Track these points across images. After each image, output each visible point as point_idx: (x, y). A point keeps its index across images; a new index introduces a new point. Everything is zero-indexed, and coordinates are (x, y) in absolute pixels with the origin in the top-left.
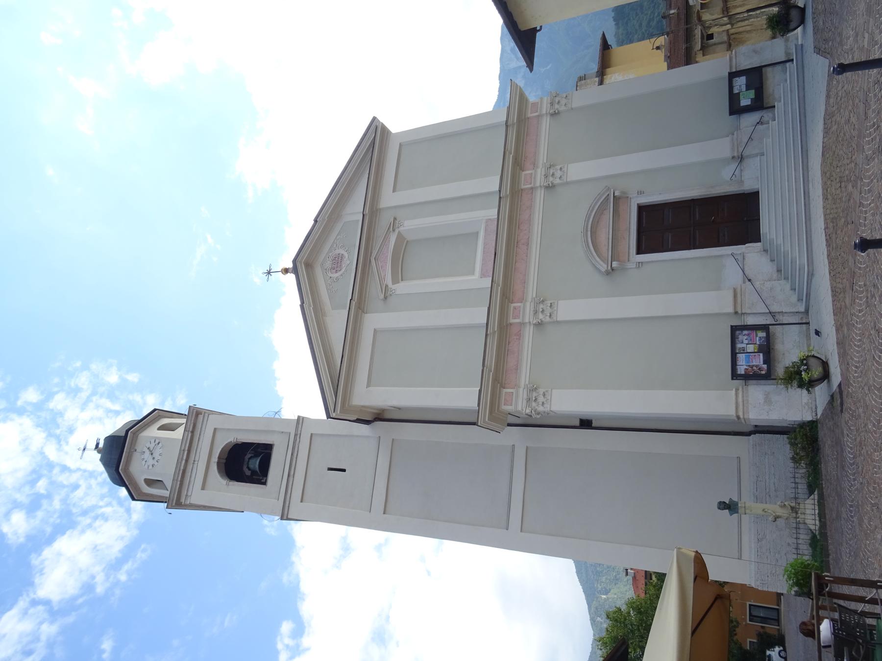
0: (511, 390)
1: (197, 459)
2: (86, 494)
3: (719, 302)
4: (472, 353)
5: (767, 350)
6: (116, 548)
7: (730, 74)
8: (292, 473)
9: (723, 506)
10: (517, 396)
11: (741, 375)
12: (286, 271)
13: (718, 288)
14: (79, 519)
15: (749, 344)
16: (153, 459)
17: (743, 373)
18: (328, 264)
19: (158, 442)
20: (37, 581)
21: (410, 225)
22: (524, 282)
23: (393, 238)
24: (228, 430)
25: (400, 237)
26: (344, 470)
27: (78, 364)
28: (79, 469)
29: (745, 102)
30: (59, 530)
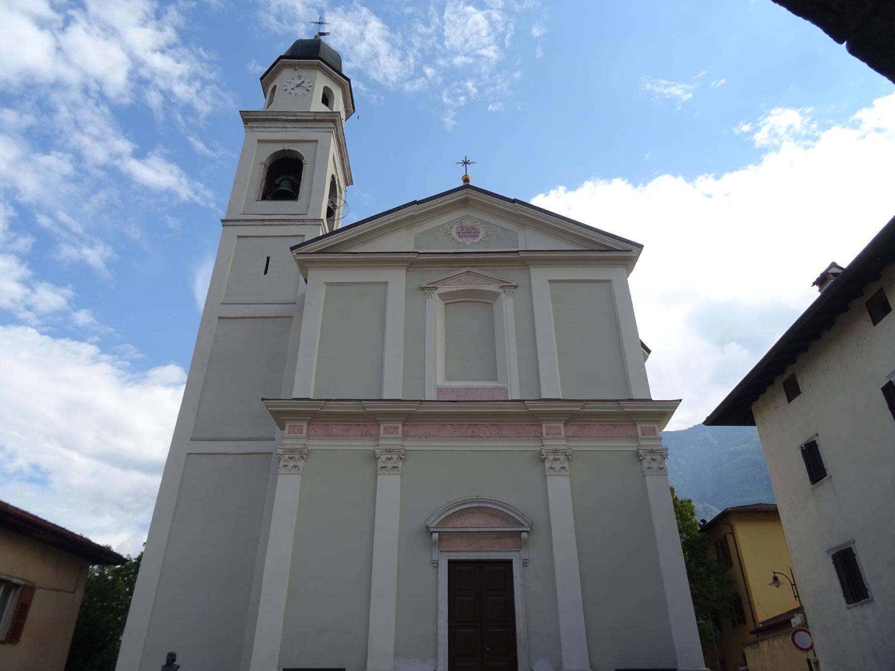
0: (305, 431)
1: (288, 130)
2: (420, 35)
4: (353, 387)
6: (377, 76)
10: (559, 439)
12: (466, 180)
13: (396, 655)
14: (399, 33)
16: (309, 90)
18: (468, 223)
19: (309, 90)
20: (339, 9)
21: (507, 305)
22: (427, 436)
25: (495, 295)
26: (266, 273)
30: (385, 18)
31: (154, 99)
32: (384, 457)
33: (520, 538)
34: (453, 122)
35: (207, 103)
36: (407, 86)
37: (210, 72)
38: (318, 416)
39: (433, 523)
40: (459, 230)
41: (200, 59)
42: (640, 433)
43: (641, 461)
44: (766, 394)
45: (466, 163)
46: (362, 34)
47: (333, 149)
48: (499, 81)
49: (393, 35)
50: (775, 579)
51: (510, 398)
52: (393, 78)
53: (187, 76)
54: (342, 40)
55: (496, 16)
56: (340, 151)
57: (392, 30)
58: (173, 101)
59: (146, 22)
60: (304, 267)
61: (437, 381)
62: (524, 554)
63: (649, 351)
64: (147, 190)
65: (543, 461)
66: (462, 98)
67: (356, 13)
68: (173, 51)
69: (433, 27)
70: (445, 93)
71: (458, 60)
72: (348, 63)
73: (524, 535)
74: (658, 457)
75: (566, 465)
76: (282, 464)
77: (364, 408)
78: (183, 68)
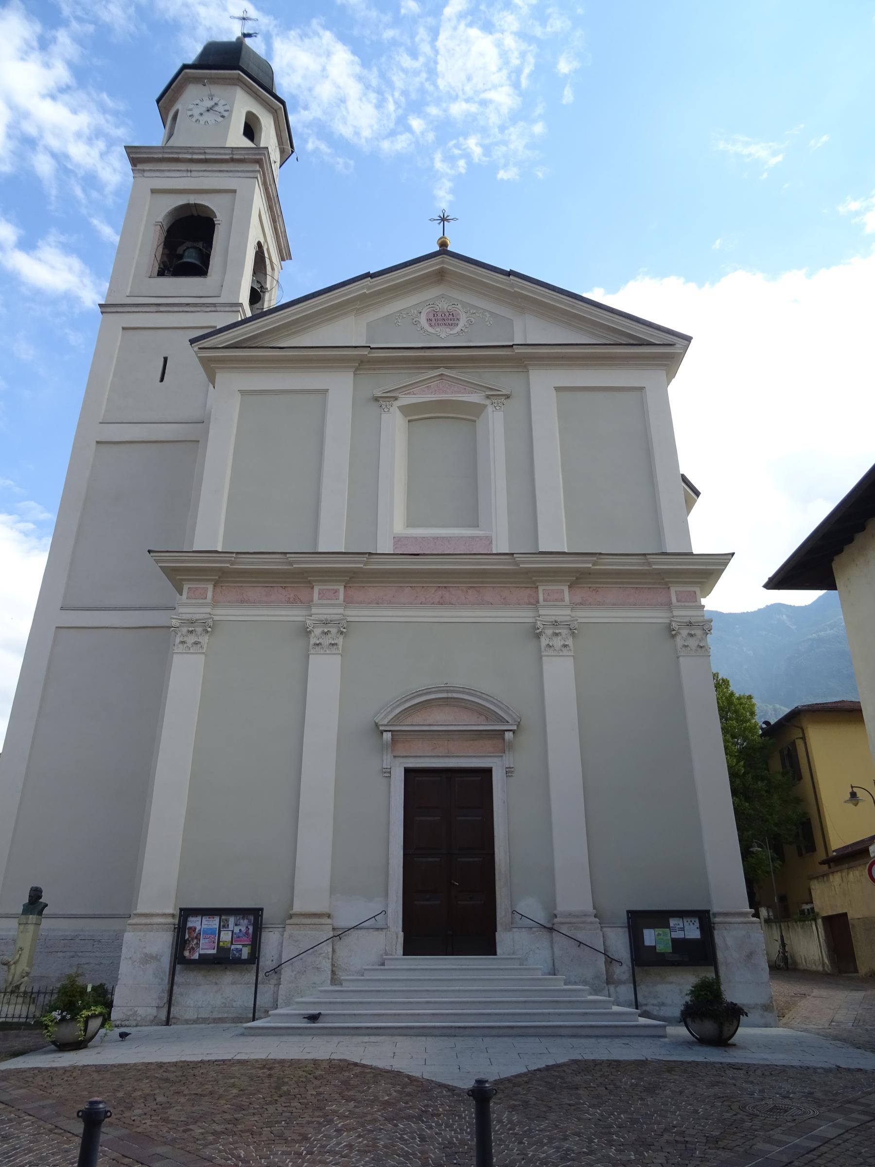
0: (210, 595)
1: (193, 174)
2: (405, 71)
3: (312, 888)
4: (279, 536)
5: (222, 961)
6: (345, 130)
8: (162, 309)
9: (36, 895)
11: (185, 922)
13: (333, 890)
14: (375, 69)
15: (232, 933)
17: (189, 925)
18: (443, 306)
20: (292, 34)
21: (495, 422)
23: (475, 398)
24: (233, 209)
25: (479, 409)
26: (162, 380)
27: (580, 11)
28: (437, 52)
29: (650, 937)
30: (356, 46)
31: (44, 165)
32: (318, 631)
33: (504, 739)
34: (450, 197)
35: (115, 170)
36: (386, 145)
37: (117, 126)
38: (227, 574)
39: (384, 720)
40: (431, 316)
41: (103, 109)
42: (674, 600)
43: (674, 636)
44: (853, 544)
45: (444, 219)
46: (324, 69)
47: (259, 202)
48: (513, 137)
49: (366, 72)
50: (853, 795)
51: (494, 552)
52: (366, 133)
53: (86, 131)
54: (297, 79)
55: (510, 41)
56: (271, 208)
57: (366, 63)
58: (69, 166)
59: (26, 53)
60: (211, 367)
61: (394, 526)
62: (508, 760)
63: (697, 494)
64: (38, 295)
65: (538, 636)
66: (462, 163)
67: (316, 39)
68: (66, 97)
69: (422, 59)
70: (438, 156)
71: (457, 109)
72: (306, 113)
73: (508, 736)
74: (698, 632)
75: (570, 642)
76: (178, 640)
77: (291, 563)
78: (83, 121)
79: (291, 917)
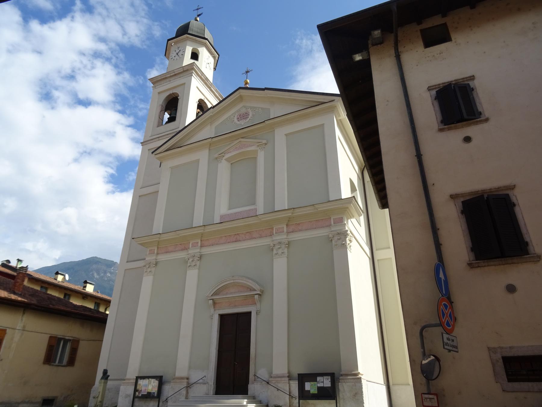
7: (137, 377)
8: (434, 87)
13: (190, 368)
29: (308, 386)
40: (239, 117)
79: (174, 379)
